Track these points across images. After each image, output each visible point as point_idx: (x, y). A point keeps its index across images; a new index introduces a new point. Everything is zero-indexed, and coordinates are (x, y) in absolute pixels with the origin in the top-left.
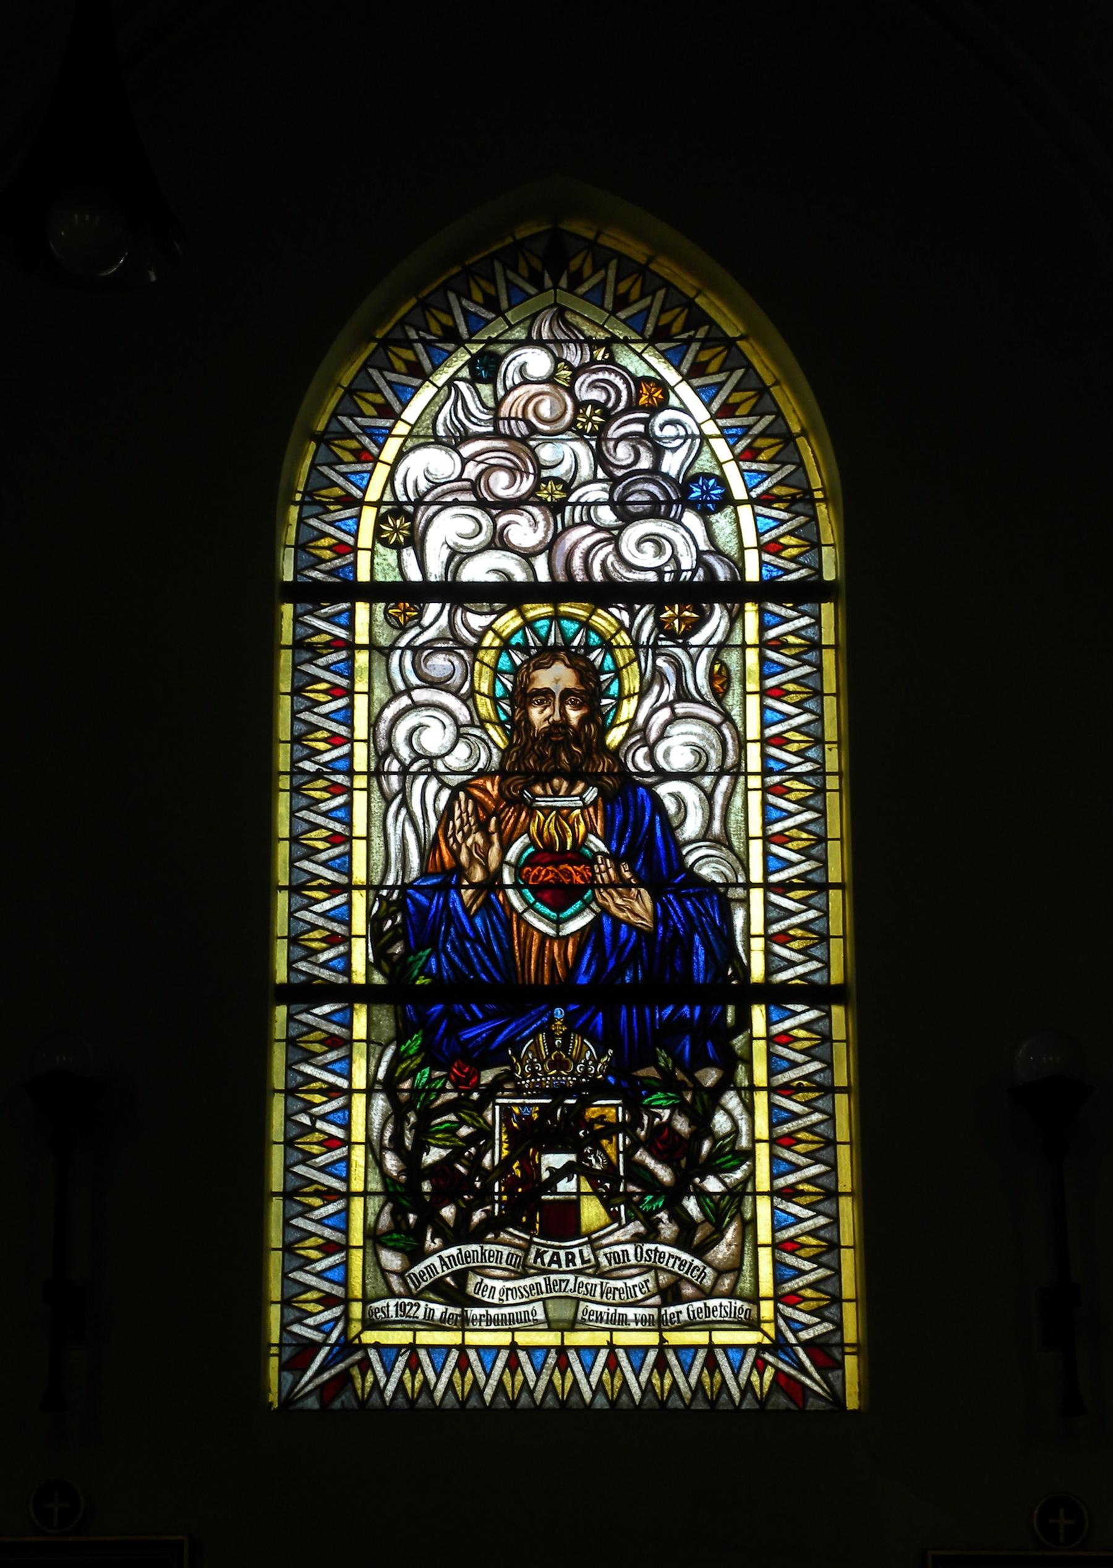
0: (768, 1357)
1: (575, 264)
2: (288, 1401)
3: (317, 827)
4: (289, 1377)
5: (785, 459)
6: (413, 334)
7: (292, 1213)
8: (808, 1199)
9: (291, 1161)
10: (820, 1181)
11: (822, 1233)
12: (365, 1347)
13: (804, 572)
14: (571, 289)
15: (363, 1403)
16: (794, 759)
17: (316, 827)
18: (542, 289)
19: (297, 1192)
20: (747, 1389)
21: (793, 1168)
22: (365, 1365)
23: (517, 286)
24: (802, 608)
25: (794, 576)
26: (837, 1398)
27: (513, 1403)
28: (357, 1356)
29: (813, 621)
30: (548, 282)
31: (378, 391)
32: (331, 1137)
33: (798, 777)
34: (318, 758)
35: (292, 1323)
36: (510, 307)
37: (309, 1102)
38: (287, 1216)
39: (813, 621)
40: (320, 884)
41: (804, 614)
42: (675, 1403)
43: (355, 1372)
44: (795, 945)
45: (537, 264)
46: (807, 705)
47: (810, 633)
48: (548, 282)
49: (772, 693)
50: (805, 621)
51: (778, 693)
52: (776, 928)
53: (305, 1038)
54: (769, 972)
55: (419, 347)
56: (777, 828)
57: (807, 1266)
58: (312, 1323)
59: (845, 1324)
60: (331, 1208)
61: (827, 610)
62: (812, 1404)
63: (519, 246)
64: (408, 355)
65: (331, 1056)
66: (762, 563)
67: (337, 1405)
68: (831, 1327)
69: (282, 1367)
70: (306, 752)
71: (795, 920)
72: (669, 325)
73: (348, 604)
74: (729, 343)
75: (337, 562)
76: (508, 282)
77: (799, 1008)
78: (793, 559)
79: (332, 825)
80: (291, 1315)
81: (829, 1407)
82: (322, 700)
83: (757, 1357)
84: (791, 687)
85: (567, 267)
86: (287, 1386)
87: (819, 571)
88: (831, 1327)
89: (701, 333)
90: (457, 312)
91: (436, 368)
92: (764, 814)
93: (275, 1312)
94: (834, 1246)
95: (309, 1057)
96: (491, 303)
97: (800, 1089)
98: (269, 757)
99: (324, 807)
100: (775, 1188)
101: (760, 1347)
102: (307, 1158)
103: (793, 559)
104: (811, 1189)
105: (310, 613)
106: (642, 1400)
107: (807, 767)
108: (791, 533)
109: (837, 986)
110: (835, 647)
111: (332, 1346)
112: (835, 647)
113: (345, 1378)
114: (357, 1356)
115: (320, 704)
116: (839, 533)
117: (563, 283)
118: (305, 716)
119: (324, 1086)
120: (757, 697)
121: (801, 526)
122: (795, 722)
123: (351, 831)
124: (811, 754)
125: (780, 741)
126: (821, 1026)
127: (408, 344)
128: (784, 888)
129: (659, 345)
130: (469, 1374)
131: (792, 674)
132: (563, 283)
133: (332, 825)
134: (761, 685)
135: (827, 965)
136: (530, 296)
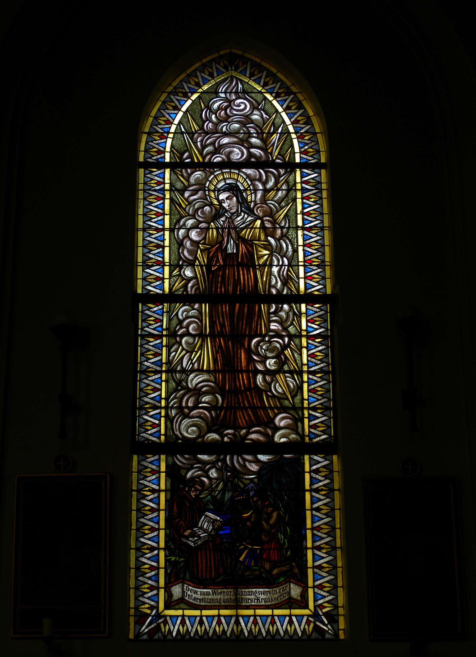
0: (311, 619)
2: (138, 635)
3: (151, 316)
4: (138, 627)
7: (139, 516)
9: (145, 220)
10: (328, 486)
12: (165, 616)
13: (322, 330)
14: (235, 70)
15: (164, 636)
17: (145, 583)
18: (228, 70)
19: (141, 490)
20: (304, 631)
21: (320, 558)
22: (165, 623)
23: (219, 69)
24: (315, 171)
25: (313, 161)
26: (336, 634)
29: (332, 539)
31: (173, 102)
34: (147, 498)
35: (140, 518)
37: (145, 475)
38: (138, 537)
39: (332, 539)
40: (152, 371)
41: (316, 173)
42: (277, 637)
45: (227, 63)
46: (318, 234)
47: (318, 179)
48: (230, 69)
49: (306, 214)
51: (308, 214)
53: (149, 213)
54: (306, 289)
56: (318, 543)
57: (322, 497)
58: (152, 352)
59: (338, 558)
62: (327, 636)
66: (301, 157)
67: (156, 637)
68: (329, 481)
69: (136, 623)
75: (160, 141)
76: (216, 68)
77: (316, 293)
78: (320, 395)
80: (146, 219)
81: (333, 637)
82: (151, 375)
83: (307, 619)
86: (137, 631)
87: (320, 160)
88: (329, 481)
90: (200, 77)
92: (304, 254)
94: (323, 246)
95: (149, 267)
97: (318, 373)
98: (137, 142)
99: (148, 575)
100: (314, 546)
101: (309, 616)
102: (144, 497)
103: (320, 395)
108: (310, 148)
109: (323, 163)
110: (342, 587)
111: (153, 616)
113: (158, 628)
115: (148, 430)
116: (327, 147)
118: (149, 176)
119: (149, 547)
120: (303, 280)
121: (316, 177)
122: (319, 384)
123: (165, 150)
124: (324, 360)
126: (331, 524)
128: (309, 229)
131: (319, 384)
132: (233, 69)
134: (302, 196)
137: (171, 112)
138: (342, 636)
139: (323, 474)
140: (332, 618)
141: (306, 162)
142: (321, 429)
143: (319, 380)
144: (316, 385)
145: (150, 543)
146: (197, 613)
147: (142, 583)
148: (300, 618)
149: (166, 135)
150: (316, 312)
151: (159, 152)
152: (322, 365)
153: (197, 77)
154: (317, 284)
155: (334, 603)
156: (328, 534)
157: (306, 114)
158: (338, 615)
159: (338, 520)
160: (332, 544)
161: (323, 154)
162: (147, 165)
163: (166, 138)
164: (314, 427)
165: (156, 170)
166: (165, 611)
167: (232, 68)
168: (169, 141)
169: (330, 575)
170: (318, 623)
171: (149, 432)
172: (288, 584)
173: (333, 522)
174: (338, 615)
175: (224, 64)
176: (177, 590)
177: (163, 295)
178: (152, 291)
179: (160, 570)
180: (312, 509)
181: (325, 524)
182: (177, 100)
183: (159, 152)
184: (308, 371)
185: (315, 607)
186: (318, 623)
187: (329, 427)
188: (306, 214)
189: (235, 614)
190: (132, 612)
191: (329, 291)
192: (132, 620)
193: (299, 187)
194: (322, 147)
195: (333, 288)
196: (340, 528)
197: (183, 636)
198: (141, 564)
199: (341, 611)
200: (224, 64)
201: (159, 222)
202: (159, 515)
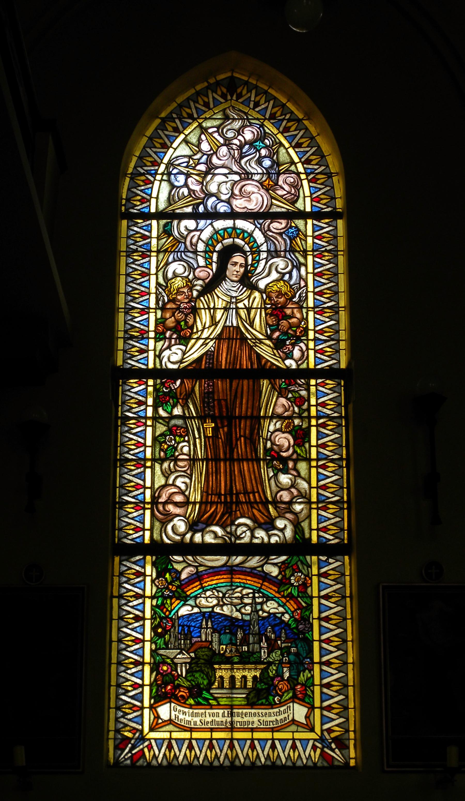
1: (239, 91)
5: (322, 164)
6: (174, 116)
8: (328, 315)
11: (331, 233)
16: (331, 538)
17: (128, 680)
18: (226, 100)
27: (211, 763)
28: (146, 744)
30: (229, 97)
32: (136, 683)
33: (326, 251)
36: (214, 107)
41: (337, 561)
43: (146, 750)
44: (326, 277)
45: (225, 90)
48: (229, 97)
50: (338, 563)
52: (317, 233)
55: (177, 121)
57: (334, 672)
60: (137, 646)
61: (340, 223)
62: (336, 763)
63: (218, 83)
64: (174, 125)
65: (136, 625)
70: (124, 691)
71: (325, 268)
72: (276, 113)
73: (141, 557)
74: (299, 121)
79: (136, 590)
84: (331, 572)
85: (236, 91)
89: (288, 117)
91: (184, 129)
93: (134, 159)
96: (207, 105)
101: (315, 740)
104: (328, 292)
105: (127, 560)
106: (265, 762)
107: (337, 498)
112: (353, 663)
114: (146, 744)
117: (234, 98)
121: (331, 230)
124: (336, 389)
125: (325, 487)
127: (173, 120)
129: (272, 121)
130: (193, 752)
132: (234, 98)
133: (136, 590)
135: (339, 362)
136: (222, 103)
137: (158, 150)
138: (352, 763)
139: (332, 577)
140: (341, 743)
141: (319, 211)
142: (331, 448)
143: (332, 516)
144: (328, 523)
145: (134, 634)
146: (187, 735)
147: (124, 680)
148: (304, 742)
149: (148, 253)
150: (325, 284)
151: (138, 445)
152: (331, 362)
153: (190, 108)
154: (326, 226)
155: (344, 726)
156: (339, 670)
157: (319, 153)
158: (349, 739)
159: (351, 675)
160: (344, 658)
161: (339, 202)
162: (131, 217)
163: (150, 256)
164: (324, 488)
165: (142, 221)
166: (150, 733)
167: (232, 96)
168: (154, 260)
169: (341, 717)
170: (326, 750)
171: (134, 431)
172: (291, 704)
173: (346, 677)
174: (349, 739)
175: (222, 92)
176: (164, 711)
177: (148, 369)
178: (135, 366)
179: (145, 687)
180: (320, 619)
181: (336, 636)
182: (167, 136)
183: (143, 201)
184: (314, 349)
185: (322, 731)
186: (326, 750)
187: (343, 575)
188: (323, 530)
189: (229, 737)
190: (111, 735)
191: (343, 365)
192: (111, 744)
193: (311, 335)
194: (339, 192)
195: (349, 364)
196: (352, 641)
197: (170, 764)
198: (123, 635)
199: (352, 735)
200: (222, 92)
201: (142, 361)
202: (143, 647)
